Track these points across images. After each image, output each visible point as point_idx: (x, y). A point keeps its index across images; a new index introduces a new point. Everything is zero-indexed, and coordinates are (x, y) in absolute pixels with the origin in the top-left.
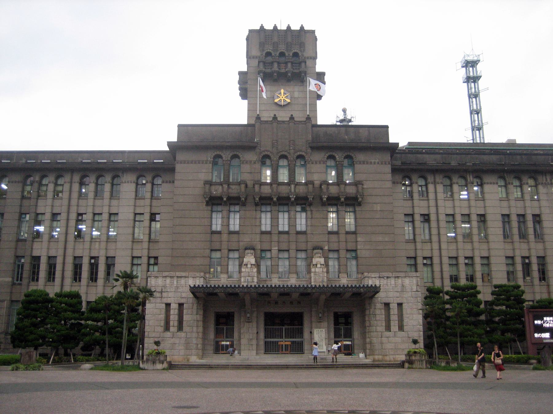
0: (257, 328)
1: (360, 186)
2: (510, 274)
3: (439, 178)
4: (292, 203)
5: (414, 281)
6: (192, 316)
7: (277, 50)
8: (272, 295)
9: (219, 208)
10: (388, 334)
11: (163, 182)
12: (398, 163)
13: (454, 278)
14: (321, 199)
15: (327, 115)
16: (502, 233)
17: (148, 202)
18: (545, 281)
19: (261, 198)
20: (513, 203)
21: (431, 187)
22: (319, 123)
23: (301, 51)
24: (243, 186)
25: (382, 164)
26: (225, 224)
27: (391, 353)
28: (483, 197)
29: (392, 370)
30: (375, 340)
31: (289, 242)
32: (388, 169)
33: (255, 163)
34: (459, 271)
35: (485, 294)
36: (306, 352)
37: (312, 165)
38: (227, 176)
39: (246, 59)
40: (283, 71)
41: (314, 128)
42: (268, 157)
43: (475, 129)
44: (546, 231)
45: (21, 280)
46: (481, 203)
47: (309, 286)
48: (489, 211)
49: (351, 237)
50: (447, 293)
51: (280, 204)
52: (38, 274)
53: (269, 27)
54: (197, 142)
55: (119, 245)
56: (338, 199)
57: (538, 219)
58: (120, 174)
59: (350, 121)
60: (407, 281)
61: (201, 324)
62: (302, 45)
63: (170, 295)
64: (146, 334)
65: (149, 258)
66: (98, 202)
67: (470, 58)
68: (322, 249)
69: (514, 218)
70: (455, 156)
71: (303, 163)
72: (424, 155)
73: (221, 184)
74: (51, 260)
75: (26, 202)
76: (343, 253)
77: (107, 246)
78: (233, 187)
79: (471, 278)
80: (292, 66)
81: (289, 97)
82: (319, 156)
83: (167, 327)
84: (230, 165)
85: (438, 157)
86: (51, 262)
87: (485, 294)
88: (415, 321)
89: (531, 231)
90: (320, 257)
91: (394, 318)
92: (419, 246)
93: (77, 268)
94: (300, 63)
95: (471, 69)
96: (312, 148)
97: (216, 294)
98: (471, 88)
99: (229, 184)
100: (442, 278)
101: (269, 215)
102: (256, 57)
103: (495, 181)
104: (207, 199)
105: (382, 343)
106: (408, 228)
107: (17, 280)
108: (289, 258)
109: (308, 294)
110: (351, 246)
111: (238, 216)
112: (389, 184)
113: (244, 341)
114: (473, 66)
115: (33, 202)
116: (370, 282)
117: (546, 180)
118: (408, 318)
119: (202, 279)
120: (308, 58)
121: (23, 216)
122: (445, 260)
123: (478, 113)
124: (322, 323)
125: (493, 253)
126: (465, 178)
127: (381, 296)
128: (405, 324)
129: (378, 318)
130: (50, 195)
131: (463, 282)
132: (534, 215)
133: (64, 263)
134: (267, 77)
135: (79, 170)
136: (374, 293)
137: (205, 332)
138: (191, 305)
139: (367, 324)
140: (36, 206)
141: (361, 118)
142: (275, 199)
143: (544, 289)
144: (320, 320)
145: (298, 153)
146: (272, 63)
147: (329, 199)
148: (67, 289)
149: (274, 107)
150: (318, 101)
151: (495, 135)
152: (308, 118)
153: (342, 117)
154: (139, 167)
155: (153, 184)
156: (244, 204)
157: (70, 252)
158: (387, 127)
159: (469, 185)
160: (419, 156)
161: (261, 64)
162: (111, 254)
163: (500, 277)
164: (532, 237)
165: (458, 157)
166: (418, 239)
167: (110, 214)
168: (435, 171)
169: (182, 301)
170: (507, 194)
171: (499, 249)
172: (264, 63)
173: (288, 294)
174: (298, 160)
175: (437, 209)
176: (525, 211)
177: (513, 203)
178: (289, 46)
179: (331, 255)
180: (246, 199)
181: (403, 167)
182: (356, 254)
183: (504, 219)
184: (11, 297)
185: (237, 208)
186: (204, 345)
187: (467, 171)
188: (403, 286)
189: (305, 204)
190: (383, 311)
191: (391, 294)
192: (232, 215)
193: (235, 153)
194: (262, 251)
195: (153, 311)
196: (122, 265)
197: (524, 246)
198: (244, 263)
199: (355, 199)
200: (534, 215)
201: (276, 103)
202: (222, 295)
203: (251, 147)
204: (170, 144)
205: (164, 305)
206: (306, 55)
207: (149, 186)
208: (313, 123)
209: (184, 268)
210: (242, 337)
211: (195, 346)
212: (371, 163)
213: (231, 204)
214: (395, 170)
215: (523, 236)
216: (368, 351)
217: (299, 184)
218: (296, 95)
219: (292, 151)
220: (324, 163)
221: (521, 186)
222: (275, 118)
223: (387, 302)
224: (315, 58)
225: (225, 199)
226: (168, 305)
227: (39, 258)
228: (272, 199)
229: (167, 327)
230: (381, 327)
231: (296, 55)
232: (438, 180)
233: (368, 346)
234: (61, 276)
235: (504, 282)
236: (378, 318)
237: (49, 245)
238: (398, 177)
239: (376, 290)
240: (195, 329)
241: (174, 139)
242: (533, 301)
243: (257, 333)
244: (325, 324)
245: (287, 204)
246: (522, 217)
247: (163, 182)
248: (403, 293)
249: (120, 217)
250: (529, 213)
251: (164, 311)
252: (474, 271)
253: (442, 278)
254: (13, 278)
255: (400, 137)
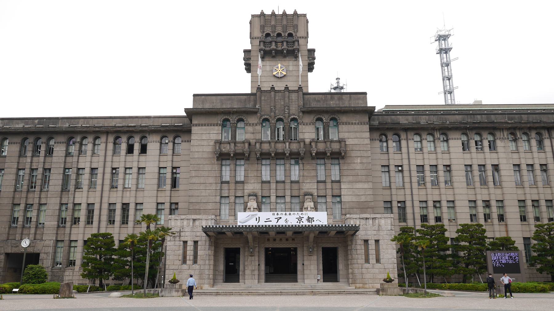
0: (259, 261)
1: (343, 143)
2: (473, 217)
3: (410, 135)
4: (287, 157)
5: (389, 221)
6: (204, 251)
7: (275, 32)
8: (270, 233)
9: (228, 162)
10: (367, 265)
11: (182, 141)
12: (376, 123)
13: (424, 218)
14: (311, 154)
15: (318, 83)
16: (465, 180)
17: (170, 158)
18: (503, 221)
19: (261, 154)
20: (522, 155)
21: (404, 143)
22: (310, 91)
23: (295, 32)
24: (247, 145)
25: (361, 124)
26: (232, 175)
27: (370, 282)
28: (448, 150)
29: (126, 298)
30: (356, 271)
31: (229, 190)
32: (367, 127)
33: (256, 125)
34: (442, 213)
35: (451, 233)
36: (299, 280)
37: (304, 126)
38: (234, 136)
39: (249, 40)
40: (280, 49)
41: (305, 96)
42: (266, 120)
43: (447, 93)
44: (503, 179)
45: (65, 223)
46: (447, 156)
47: (344, 226)
48: (454, 162)
49: (336, 186)
50: (418, 231)
51: (277, 159)
52: (92, 218)
53: (268, 12)
54: (210, 110)
55: (146, 193)
56: (324, 153)
57: (544, 168)
58: (147, 135)
59: (342, 88)
60: (383, 222)
61: (212, 257)
62: (296, 27)
63: (187, 234)
64: (167, 266)
65: (171, 203)
66: (116, 159)
67: (442, 33)
68: (312, 195)
69: (475, 168)
70: (424, 116)
71: (335, 124)
72: (398, 117)
73: (269, 142)
74: (90, 206)
75: (69, 159)
76: (329, 199)
77: (136, 194)
78: (239, 145)
79: (438, 219)
80: (287, 45)
81: (285, 70)
82: (308, 119)
83: (184, 261)
84: (236, 127)
85: (410, 118)
86: (90, 208)
87: (451, 233)
88: (390, 254)
89: (490, 179)
90: (310, 202)
91: (372, 252)
92: (394, 192)
93: (112, 211)
94: (294, 42)
95: (443, 42)
96: (304, 112)
97: (224, 233)
98: (443, 58)
99: (235, 143)
100: (414, 219)
101: (282, 168)
102: (258, 38)
103: (459, 137)
104: (217, 155)
105: (362, 274)
106: (384, 178)
107: (62, 224)
108: (326, 202)
109: (300, 233)
110: (336, 192)
111: (243, 168)
112: (368, 141)
113: (248, 272)
114: (444, 40)
115: (75, 159)
116: (352, 223)
117: (504, 136)
118: (384, 252)
119: (213, 221)
120: (300, 38)
121: (67, 170)
122: (417, 204)
123: (449, 79)
124: (312, 257)
125: (457, 198)
126: (433, 135)
127: (361, 234)
128: (381, 257)
129: (359, 252)
130: (89, 153)
131: (432, 222)
132: (541, 165)
133: (100, 209)
134: (266, 54)
135: (127, 132)
136: (354, 232)
137: (215, 265)
138: (204, 242)
139: (350, 257)
140: (78, 162)
141: (351, 86)
142: (273, 155)
143: (503, 228)
144: (310, 254)
145: (292, 117)
146: (271, 42)
147: (317, 153)
148: (103, 231)
149: (273, 79)
150: (309, 74)
151: (464, 98)
152: (300, 88)
153: (336, 85)
154: (162, 129)
155: (174, 143)
156: (248, 159)
157: (105, 200)
158: (365, 94)
159: (436, 141)
160: (393, 117)
161: (262, 44)
162: (90, 201)
163: (464, 219)
164: (491, 184)
165: (427, 117)
166: (393, 186)
167: (139, 168)
168: (406, 130)
169: (196, 239)
170: (435, 147)
171: (461, 193)
172: (264, 42)
173: (283, 233)
174: (292, 122)
175: (409, 161)
176: (485, 162)
177: (426, 156)
178: (285, 28)
179: (320, 200)
180: (249, 155)
181: (379, 127)
182: (341, 199)
183: (466, 169)
184: (57, 237)
185: (242, 162)
186: (214, 275)
187: (434, 129)
188: (379, 225)
189: (298, 158)
190: (363, 247)
191: (369, 233)
192: (224, 168)
193: (240, 117)
194: (263, 197)
195: (172, 249)
196: (149, 209)
197: (485, 191)
198: (248, 207)
199: (339, 153)
200: (541, 165)
201: (274, 76)
202: (229, 234)
203: (253, 113)
204: (187, 110)
205: (182, 243)
206: (299, 34)
207: (171, 145)
208: (304, 91)
209: (198, 211)
210: (246, 268)
211: (207, 276)
212: (352, 124)
213: (237, 159)
214: (372, 129)
215: (484, 182)
216: (350, 280)
217: (332, 141)
218: (291, 68)
219: (287, 115)
220: (313, 124)
221: (447, 141)
222: (273, 88)
223: (366, 239)
224: (306, 37)
225: (232, 155)
226: (185, 242)
227: (127, 204)
228: (271, 154)
229: (184, 261)
230: (361, 260)
231: (290, 35)
232: (409, 137)
233: (351, 276)
234: (98, 220)
235: (468, 222)
236: (358, 253)
237: (88, 194)
238: (376, 135)
239: (356, 229)
240: (207, 262)
241: (190, 106)
242: (493, 238)
243: (259, 265)
244: (315, 257)
245: (284, 159)
246: (434, 168)
247: (182, 141)
248: (380, 231)
249: (147, 170)
250: (427, 163)
251: (181, 247)
252: (541, 212)
253: (414, 219)
254: (58, 222)
255: (377, 101)
